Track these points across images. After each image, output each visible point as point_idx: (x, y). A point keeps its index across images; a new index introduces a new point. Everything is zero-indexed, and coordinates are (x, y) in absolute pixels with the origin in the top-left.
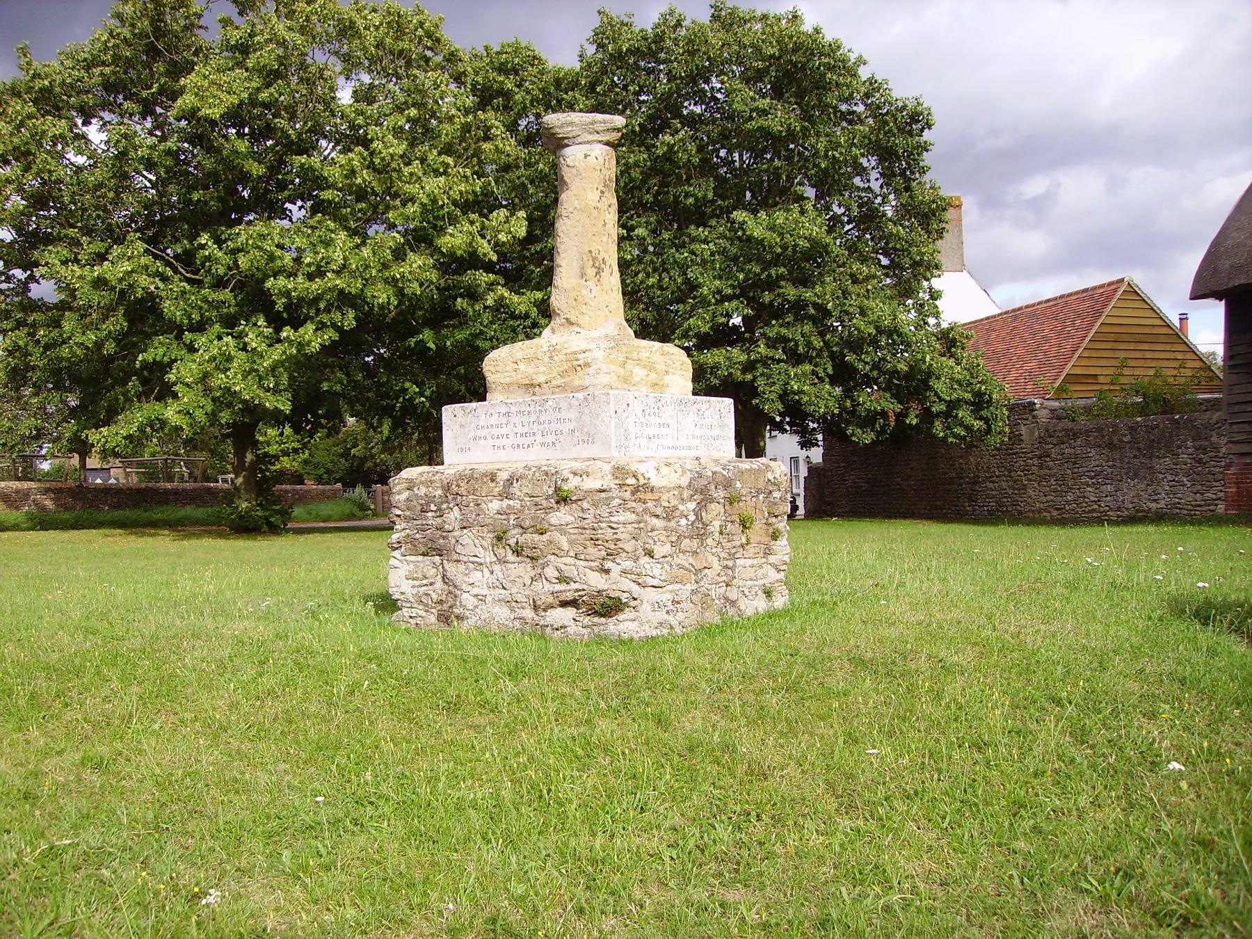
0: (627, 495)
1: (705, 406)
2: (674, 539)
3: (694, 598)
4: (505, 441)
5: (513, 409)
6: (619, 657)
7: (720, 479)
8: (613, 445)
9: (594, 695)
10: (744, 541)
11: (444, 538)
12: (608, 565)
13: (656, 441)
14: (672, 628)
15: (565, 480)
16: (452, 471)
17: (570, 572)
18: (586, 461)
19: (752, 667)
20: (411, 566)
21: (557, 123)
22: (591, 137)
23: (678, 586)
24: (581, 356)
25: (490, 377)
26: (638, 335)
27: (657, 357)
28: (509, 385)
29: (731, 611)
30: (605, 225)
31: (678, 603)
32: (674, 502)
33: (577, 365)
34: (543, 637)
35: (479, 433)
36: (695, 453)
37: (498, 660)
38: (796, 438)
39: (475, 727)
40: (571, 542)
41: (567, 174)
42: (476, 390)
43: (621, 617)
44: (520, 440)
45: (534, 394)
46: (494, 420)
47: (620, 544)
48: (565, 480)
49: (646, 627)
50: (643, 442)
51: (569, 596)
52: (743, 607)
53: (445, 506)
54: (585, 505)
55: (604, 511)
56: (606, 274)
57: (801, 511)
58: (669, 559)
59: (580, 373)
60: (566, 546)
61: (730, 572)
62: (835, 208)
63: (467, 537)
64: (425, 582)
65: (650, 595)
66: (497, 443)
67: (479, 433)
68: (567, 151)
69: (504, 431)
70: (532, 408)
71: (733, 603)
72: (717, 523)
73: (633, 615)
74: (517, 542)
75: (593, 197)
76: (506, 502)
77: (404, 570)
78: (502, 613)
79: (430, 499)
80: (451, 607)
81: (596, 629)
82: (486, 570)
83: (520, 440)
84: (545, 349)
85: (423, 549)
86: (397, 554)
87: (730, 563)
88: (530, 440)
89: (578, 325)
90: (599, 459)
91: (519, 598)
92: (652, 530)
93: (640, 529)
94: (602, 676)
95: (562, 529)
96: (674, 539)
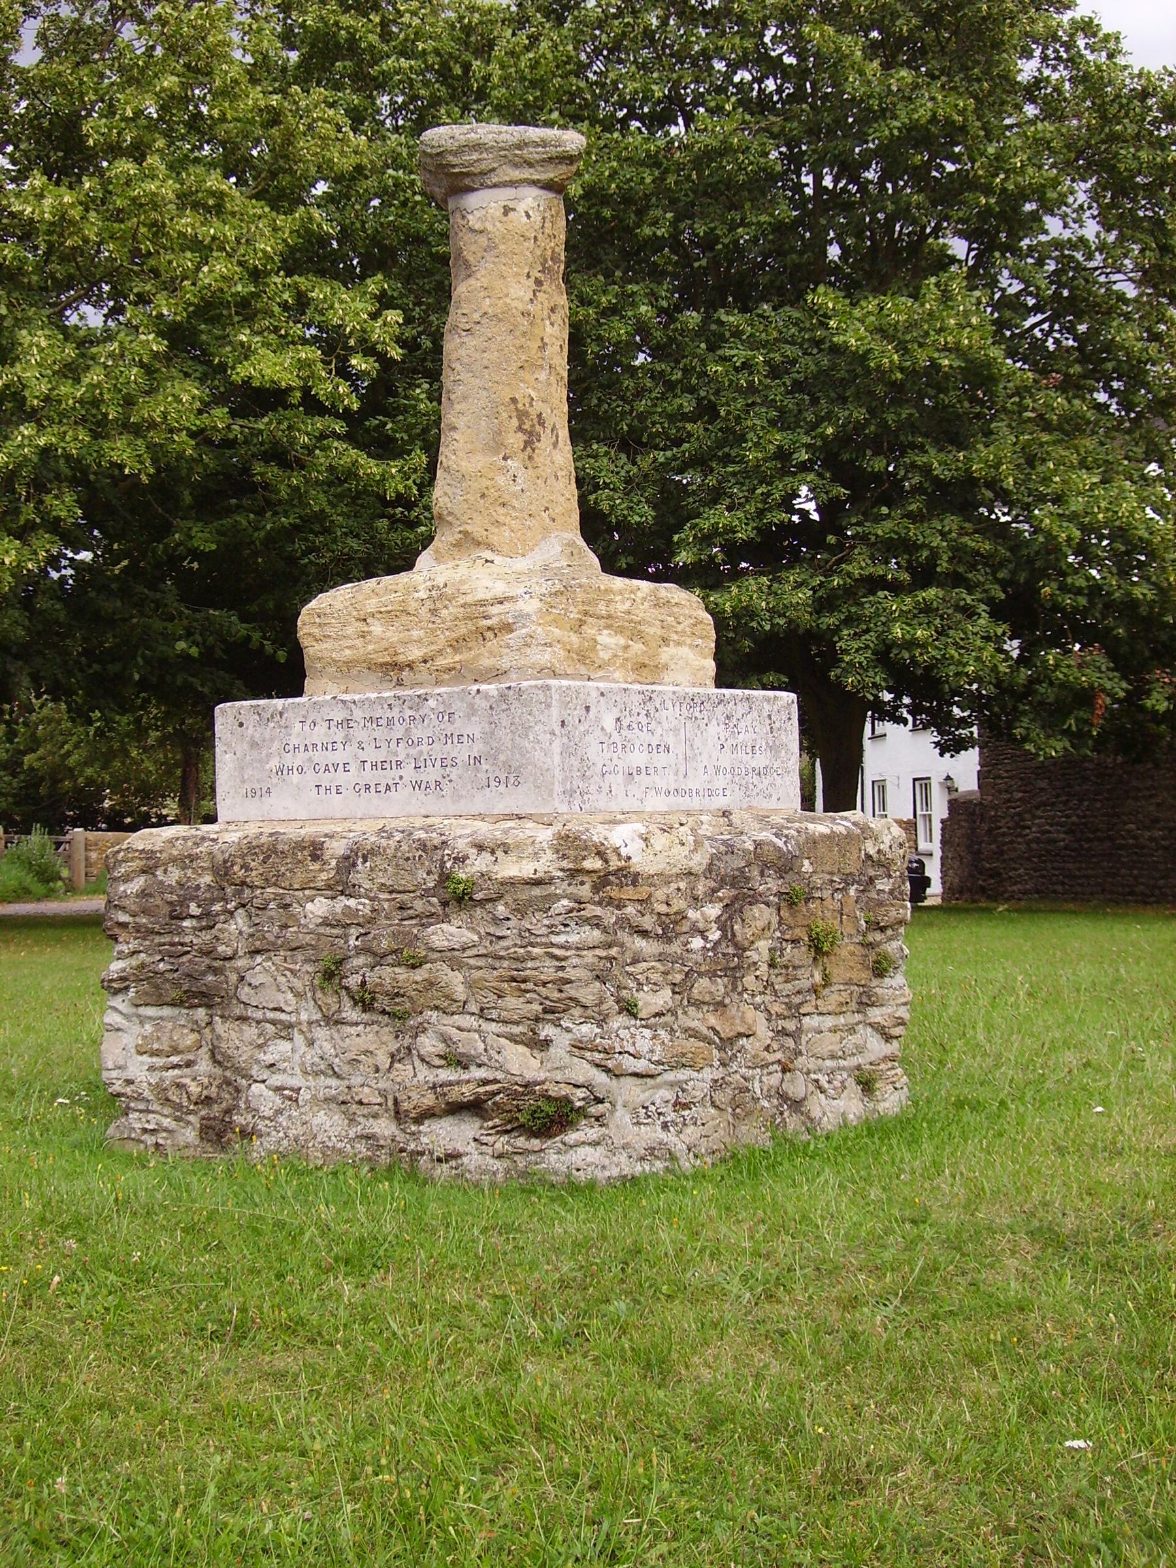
0: (585, 891)
1: (741, 709)
2: (678, 978)
3: (719, 1097)
4: (341, 777)
5: (358, 714)
6: (571, 1223)
7: (772, 856)
8: (558, 788)
9: (516, 1308)
10: (818, 978)
11: (216, 971)
12: (547, 1031)
13: (643, 780)
14: (673, 1157)
15: (461, 860)
16: (233, 837)
17: (472, 1044)
18: (506, 827)
19: (833, 1246)
20: (149, 1028)
21: (450, 145)
22: (516, 174)
23: (682, 1075)
24: (495, 610)
25: (312, 649)
26: (609, 566)
27: (644, 611)
28: (350, 664)
29: (793, 1122)
30: (543, 347)
31: (686, 1106)
32: (679, 904)
33: (484, 625)
34: (413, 1175)
35: (288, 760)
36: (721, 802)
37: (325, 1229)
38: (930, 737)
39: (278, 1377)
40: (470, 985)
41: (469, 247)
42: (283, 675)
43: (572, 1137)
44: (369, 776)
45: (400, 683)
46: (319, 734)
47: (570, 991)
48: (461, 860)
49: (623, 1158)
50: (617, 781)
51: (467, 1092)
52: (816, 1113)
53: (217, 907)
54: (501, 909)
55: (537, 923)
56: (546, 440)
57: (935, 888)
58: (668, 1018)
59: (492, 644)
60: (460, 992)
61: (790, 1043)
62: (1004, 279)
63: (261, 971)
64: (175, 1059)
65: (630, 1091)
66: (325, 779)
67: (288, 760)
68: (472, 201)
69: (339, 756)
70: (395, 713)
71: (797, 1105)
72: (763, 945)
73: (593, 1133)
74: (365, 982)
75: (519, 292)
76: (343, 901)
77: (131, 1037)
78: (329, 1125)
79: (187, 892)
80: (228, 1111)
81: (521, 1162)
82: (299, 1039)
83: (369, 776)
84: (423, 594)
85: (174, 994)
86: (118, 1002)
87: (791, 1025)
88: (391, 775)
89: (489, 547)
90: (529, 817)
91: (366, 1094)
92: (635, 961)
93: (611, 959)
94: (533, 1266)
95: (453, 957)
96: (678, 978)
